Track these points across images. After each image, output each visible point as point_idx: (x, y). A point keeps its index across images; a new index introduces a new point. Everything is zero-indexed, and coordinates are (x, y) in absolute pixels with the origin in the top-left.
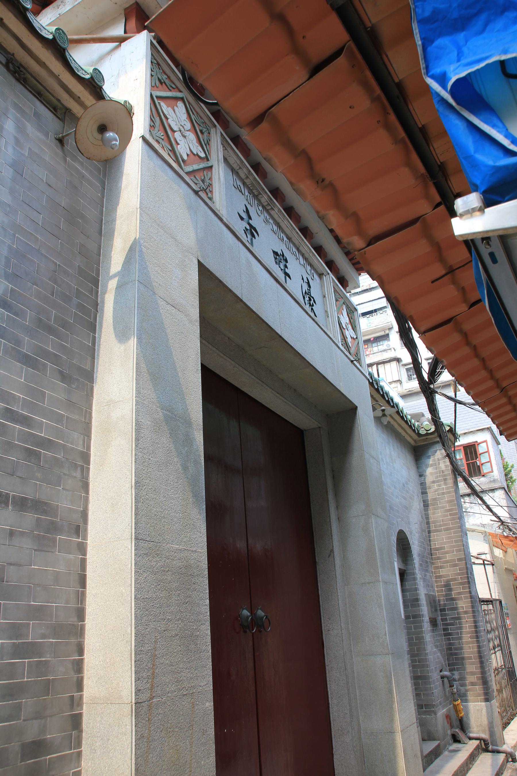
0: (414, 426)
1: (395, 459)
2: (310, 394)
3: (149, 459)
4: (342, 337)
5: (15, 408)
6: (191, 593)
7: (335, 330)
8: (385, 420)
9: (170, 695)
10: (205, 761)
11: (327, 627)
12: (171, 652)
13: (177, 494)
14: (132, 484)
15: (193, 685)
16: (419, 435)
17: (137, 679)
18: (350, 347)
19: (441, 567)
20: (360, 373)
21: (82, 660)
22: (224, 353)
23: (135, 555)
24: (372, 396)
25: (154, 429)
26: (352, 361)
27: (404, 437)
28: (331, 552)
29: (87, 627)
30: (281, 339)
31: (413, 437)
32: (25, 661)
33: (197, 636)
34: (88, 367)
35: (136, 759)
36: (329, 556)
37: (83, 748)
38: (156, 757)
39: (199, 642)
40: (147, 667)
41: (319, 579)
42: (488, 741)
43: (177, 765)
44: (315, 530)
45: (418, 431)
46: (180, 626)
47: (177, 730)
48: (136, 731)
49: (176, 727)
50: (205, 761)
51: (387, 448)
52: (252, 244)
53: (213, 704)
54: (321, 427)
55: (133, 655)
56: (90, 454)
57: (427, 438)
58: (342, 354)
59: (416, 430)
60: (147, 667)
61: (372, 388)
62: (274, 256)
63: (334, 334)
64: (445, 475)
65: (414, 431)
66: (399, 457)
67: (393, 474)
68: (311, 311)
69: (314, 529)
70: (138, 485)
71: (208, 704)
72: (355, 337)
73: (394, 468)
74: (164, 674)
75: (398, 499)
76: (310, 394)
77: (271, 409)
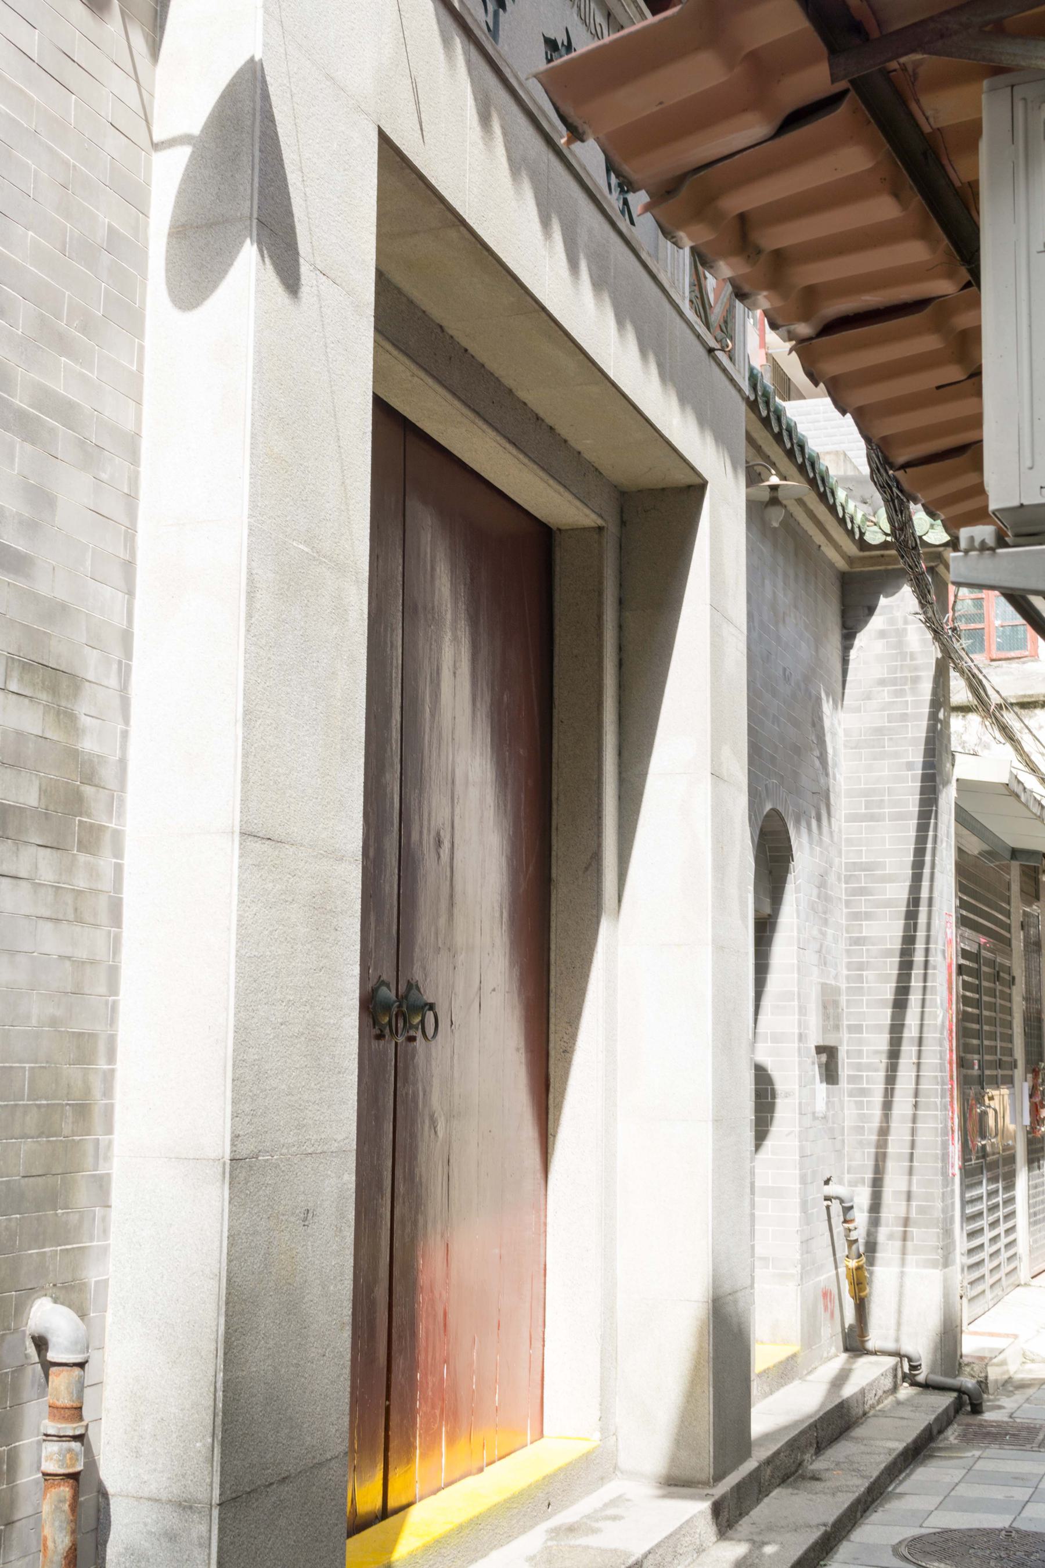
0: (852, 522)
1: (784, 613)
2: (588, 442)
3: (269, 659)
4: (694, 277)
5: (5, 538)
6: (329, 950)
7: (678, 261)
8: (775, 518)
9: (284, 1151)
10: (336, 1286)
11: (562, 1043)
12: (290, 1068)
13: (314, 734)
14: (236, 716)
15: (323, 1137)
16: (862, 544)
17: (235, 1115)
18: (711, 306)
19: (868, 916)
20: (727, 383)
21: (113, 1071)
22: (395, 342)
23: (240, 867)
24: (750, 439)
25: (278, 590)
26: (711, 351)
27: (820, 546)
28: (591, 858)
29: (122, 1008)
30: (543, 314)
31: (845, 548)
32: (25, 1067)
33: (336, 1039)
34: (130, 426)
35: (230, 1261)
36: (587, 869)
37: (111, 1239)
38: (258, 1265)
39: (337, 1052)
40: (251, 1094)
41: (553, 924)
42: (919, 1359)
43: (290, 1284)
44: (557, 799)
45: (862, 534)
46: (307, 1016)
47: (293, 1219)
48: (230, 1212)
49: (293, 1214)
50: (336, 1286)
51: (767, 582)
52: (494, 32)
53: (354, 1178)
54: (604, 527)
55: (230, 1068)
56: (133, 633)
57: (882, 556)
58: (688, 331)
59: (857, 530)
60: (251, 1094)
61: (752, 416)
62: (546, 53)
63: (673, 274)
64: (916, 668)
65: (850, 533)
66: (796, 607)
67: (773, 657)
68: (622, 212)
69: (554, 795)
70: (249, 716)
71: (346, 1177)
72: (752, 398)
73: (778, 639)
74: (277, 1110)
75: (779, 726)
76: (588, 442)
77: (482, 474)
